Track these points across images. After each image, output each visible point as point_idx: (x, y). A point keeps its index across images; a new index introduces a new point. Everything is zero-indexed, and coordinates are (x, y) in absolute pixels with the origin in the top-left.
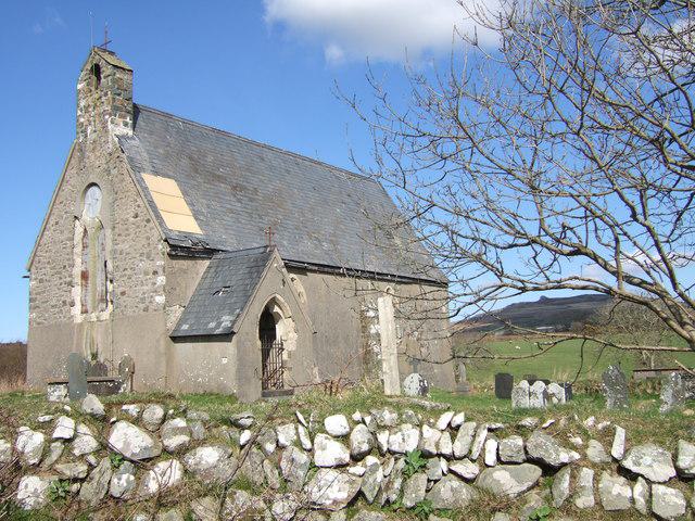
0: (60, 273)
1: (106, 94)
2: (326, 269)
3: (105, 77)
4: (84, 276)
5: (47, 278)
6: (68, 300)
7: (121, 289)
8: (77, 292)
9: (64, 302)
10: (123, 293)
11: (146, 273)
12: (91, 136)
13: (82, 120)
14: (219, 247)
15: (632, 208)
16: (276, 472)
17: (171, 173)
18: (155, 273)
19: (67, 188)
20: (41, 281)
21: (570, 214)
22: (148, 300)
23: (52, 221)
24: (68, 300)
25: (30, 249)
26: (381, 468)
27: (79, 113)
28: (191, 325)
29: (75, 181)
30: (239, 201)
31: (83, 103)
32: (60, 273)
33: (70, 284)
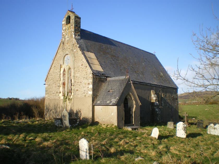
0: (56, 83)
1: (72, 25)
2: (141, 83)
3: (72, 20)
4: (64, 84)
5: (51, 84)
6: (58, 91)
7: (77, 89)
8: (61, 89)
9: (57, 92)
10: (77, 90)
11: (85, 84)
12: (67, 39)
13: (64, 34)
14: (109, 76)
15: (139, 84)
16: (183, 153)
17: (92, 51)
18: (89, 84)
19: (58, 55)
20: (49, 85)
21: (66, 95)
22: (86, 93)
23: (53, 66)
24: (58, 91)
25: (47, 74)
26: (29, 145)
27: (63, 31)
28: (101, 102)
29: (61, 53)
30: (114, 60)
31: (64, 28)
32: (56, 83)
33: (59, 86)
